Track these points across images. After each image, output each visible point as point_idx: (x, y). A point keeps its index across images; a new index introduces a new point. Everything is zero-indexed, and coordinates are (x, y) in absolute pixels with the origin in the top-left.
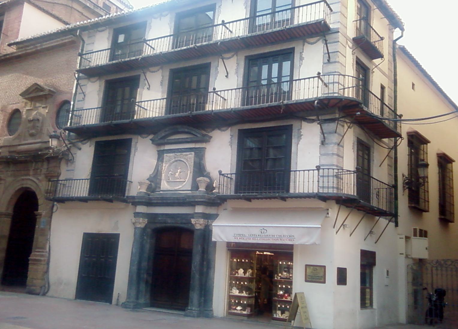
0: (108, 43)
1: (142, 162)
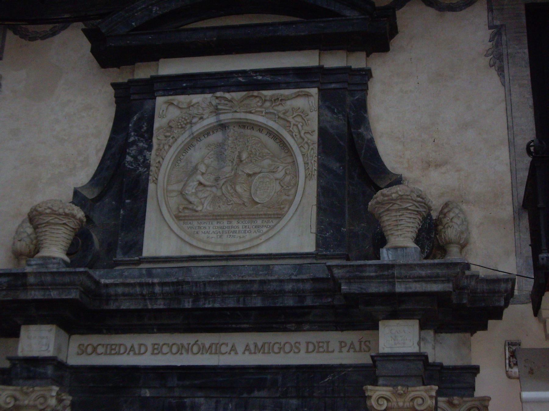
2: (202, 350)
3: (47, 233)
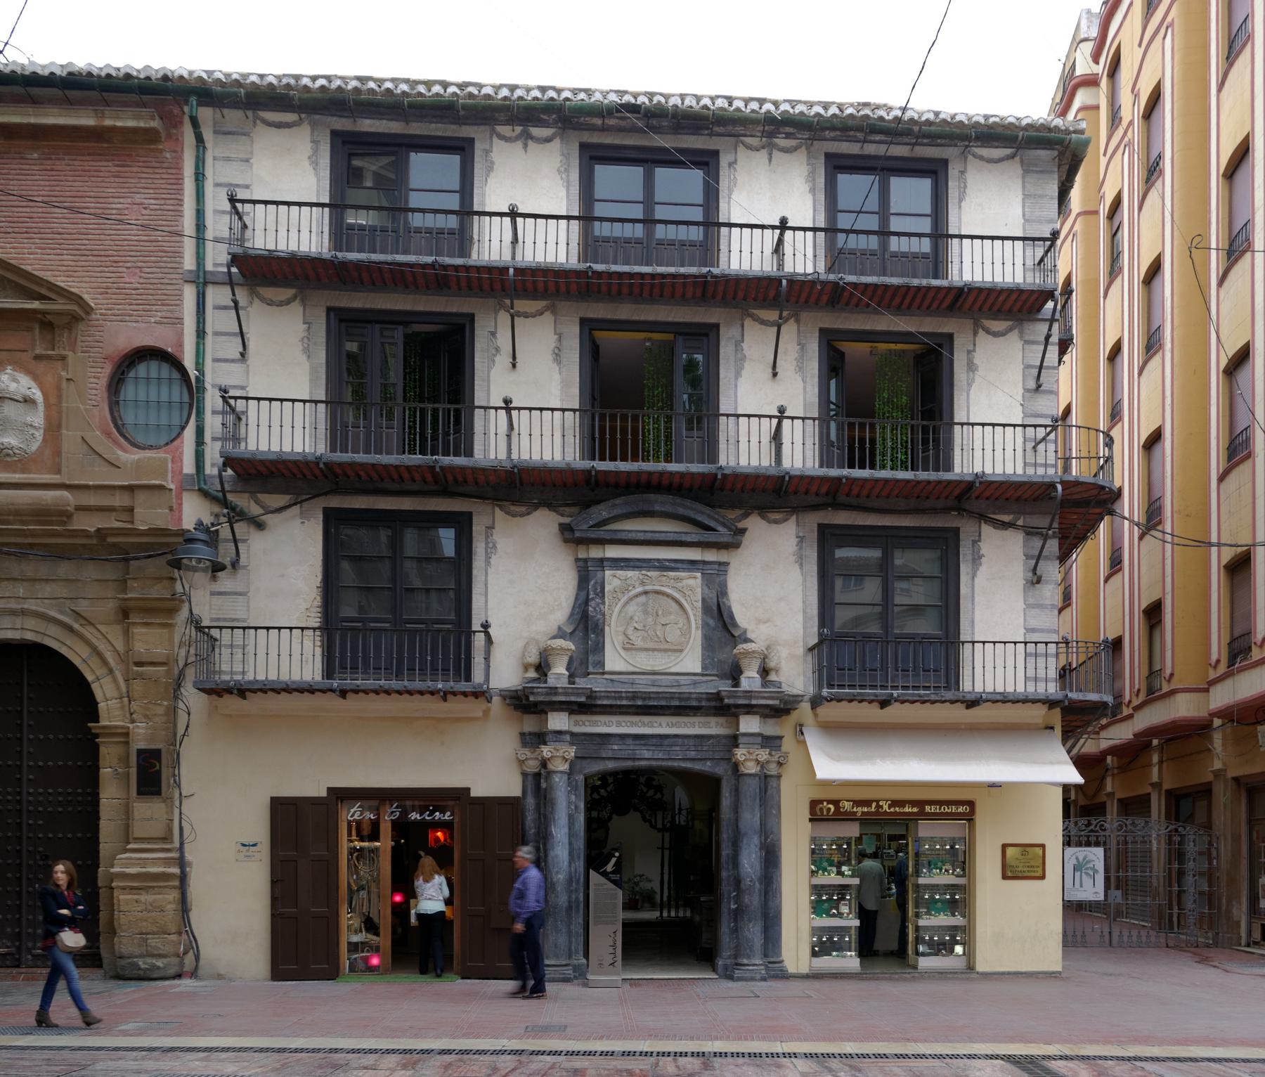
0: (317, 175)
1: (520, 591)
2: (644, 725)
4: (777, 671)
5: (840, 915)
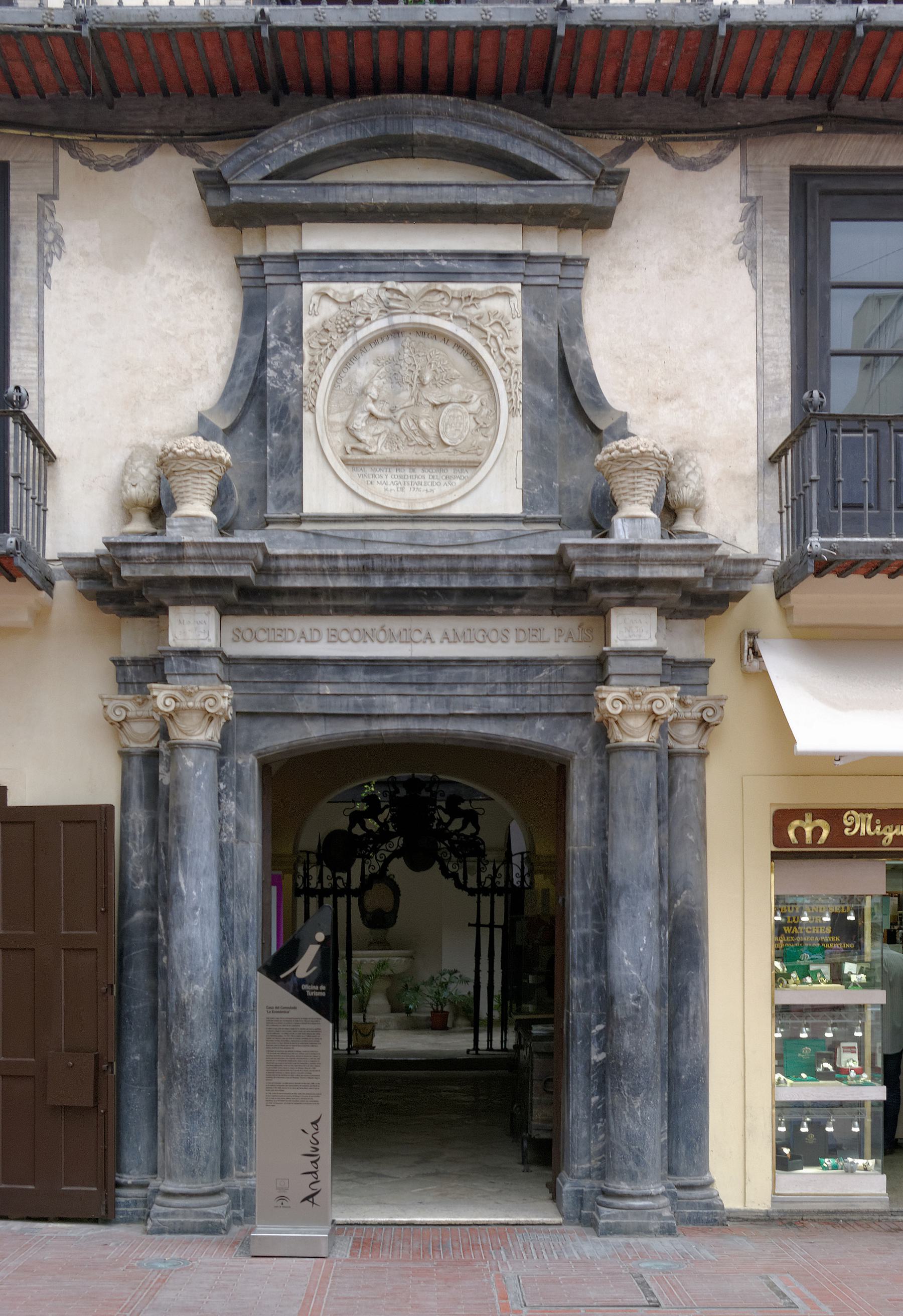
2: (392, 638)
3: (188, 483)
4: (698, 511)
5: (840, 1074)
